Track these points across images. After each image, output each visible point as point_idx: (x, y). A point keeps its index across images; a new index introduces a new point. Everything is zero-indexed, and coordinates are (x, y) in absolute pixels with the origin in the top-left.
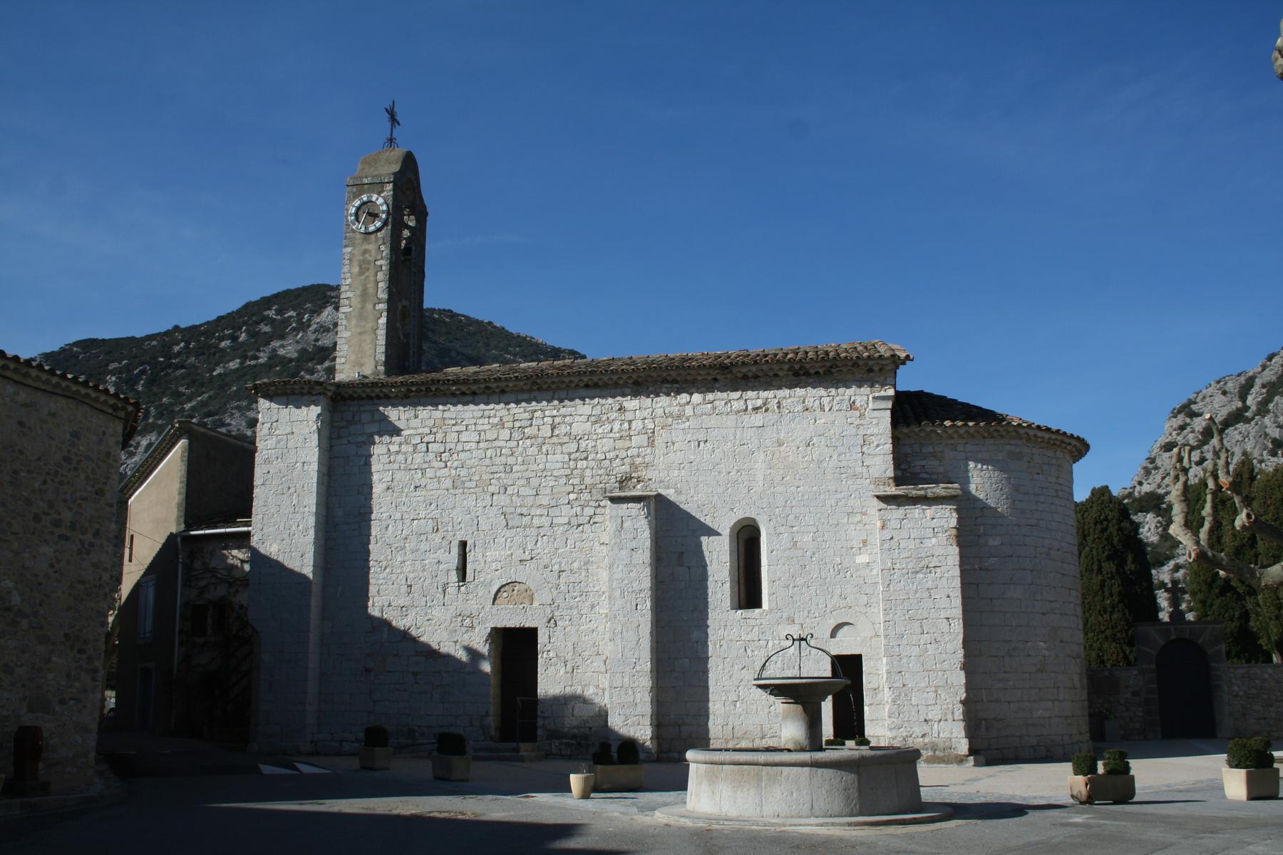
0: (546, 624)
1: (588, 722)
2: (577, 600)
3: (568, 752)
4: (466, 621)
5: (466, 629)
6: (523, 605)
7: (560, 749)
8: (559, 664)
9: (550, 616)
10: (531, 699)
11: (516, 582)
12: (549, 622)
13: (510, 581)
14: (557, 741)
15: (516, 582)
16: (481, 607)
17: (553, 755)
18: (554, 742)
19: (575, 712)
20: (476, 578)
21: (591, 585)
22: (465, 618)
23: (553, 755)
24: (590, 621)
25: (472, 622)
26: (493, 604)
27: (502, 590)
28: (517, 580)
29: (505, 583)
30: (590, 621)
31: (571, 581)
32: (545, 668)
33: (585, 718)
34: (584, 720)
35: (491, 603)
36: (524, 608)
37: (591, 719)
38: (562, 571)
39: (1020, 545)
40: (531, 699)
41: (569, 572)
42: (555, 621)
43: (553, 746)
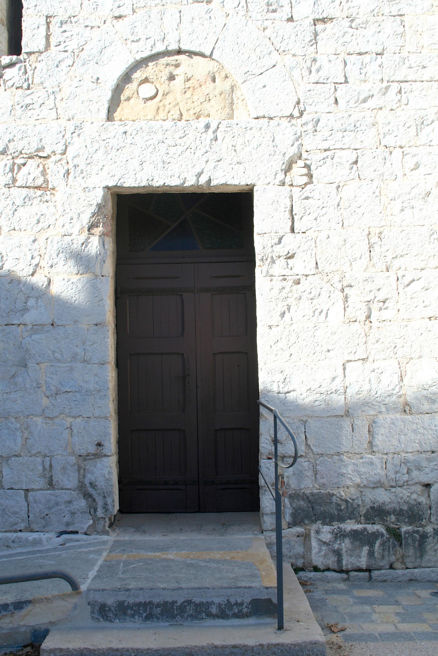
0: (281, 176)
1: (419, 468)
2: (371, 103)
3: (363, 562)
4: (24, 170)
5: (25, 191)
6: (203, 121)
7: (338, 553)
8: (325, 294)
9: (293, 151)
10: (128, 317)
11: (179, 52)
12: (288, 169)
13: (160, 48)
14: (326, 528)
15: (179, 52)
16: (70, 127)
17: (316, 569)
18: (318, 532)
19: (379, 440)
20: (53, 41)
21: (413, 60)
22: (19, 161)
23: (316, 569)
24: (417, 167)
25: (44, 173)
26: (110, 117)
27: (138, 75)
28: (184, 47)
29: (147, 54)
30: (417, 167)
31: (352, 48)
32: (281, 307)
33: (410, 456)
34: (406, 462)
35: (104, 112)
36: (207, 126)
37: (429, 460)
38: (323, 20)
39: (345, 398)
40: (128, 317)
41: (345, 22)
42: (307, 167)
43: (314, 543)
